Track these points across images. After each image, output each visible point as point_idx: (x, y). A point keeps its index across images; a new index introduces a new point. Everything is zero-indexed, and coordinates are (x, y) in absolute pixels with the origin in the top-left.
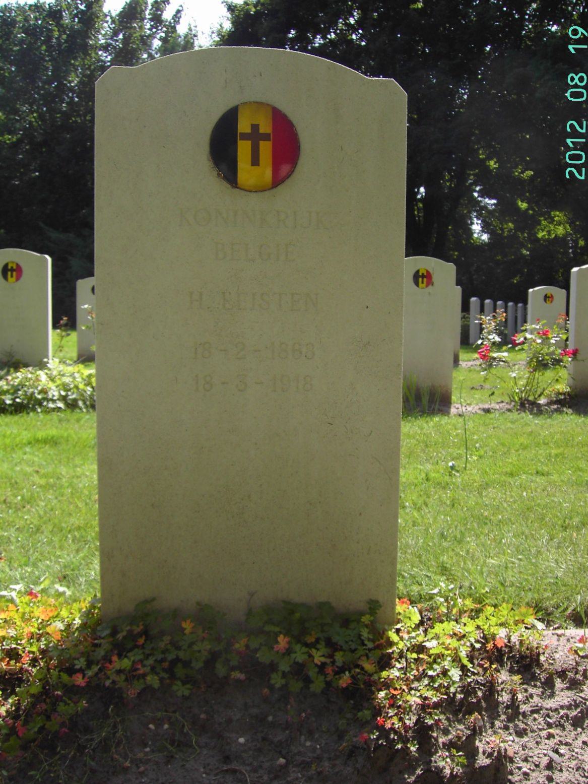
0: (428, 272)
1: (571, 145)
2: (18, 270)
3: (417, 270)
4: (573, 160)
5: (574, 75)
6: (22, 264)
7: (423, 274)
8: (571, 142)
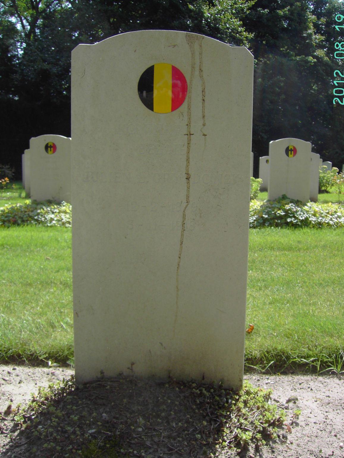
1: (336, 85)
2: (294, 151)
4: (337, 94)
5: (338, 43)
6: (56, 144)
8: (337, 83)
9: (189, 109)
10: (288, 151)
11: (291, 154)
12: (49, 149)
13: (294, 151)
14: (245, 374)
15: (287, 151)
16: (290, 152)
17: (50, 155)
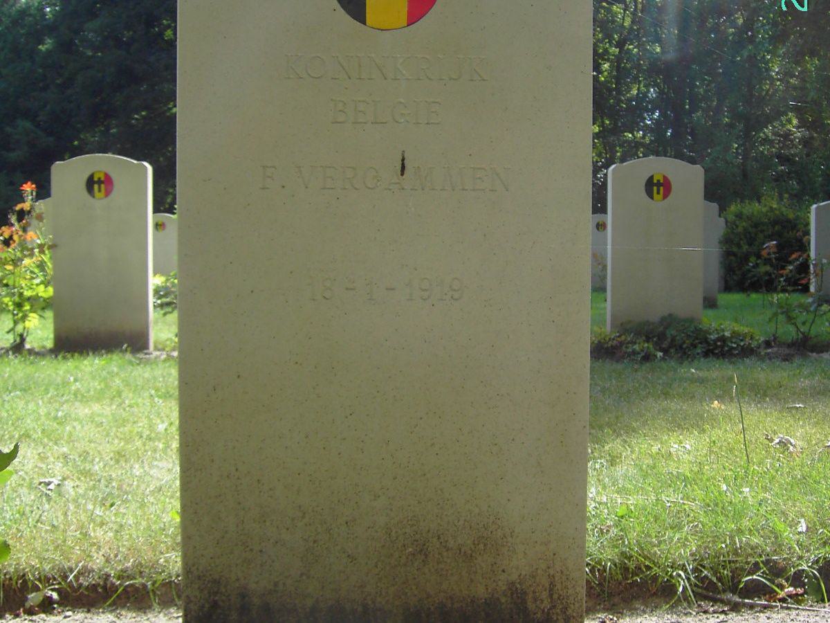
0: (665, 178)
2: (107, 181)
3: (650, 175)
7: (658, 181)
10: (651, 186)
12: (96, 187)
13: (107, 181)
14: (612, 415)
15: (650, 185)
17: (658, 202)
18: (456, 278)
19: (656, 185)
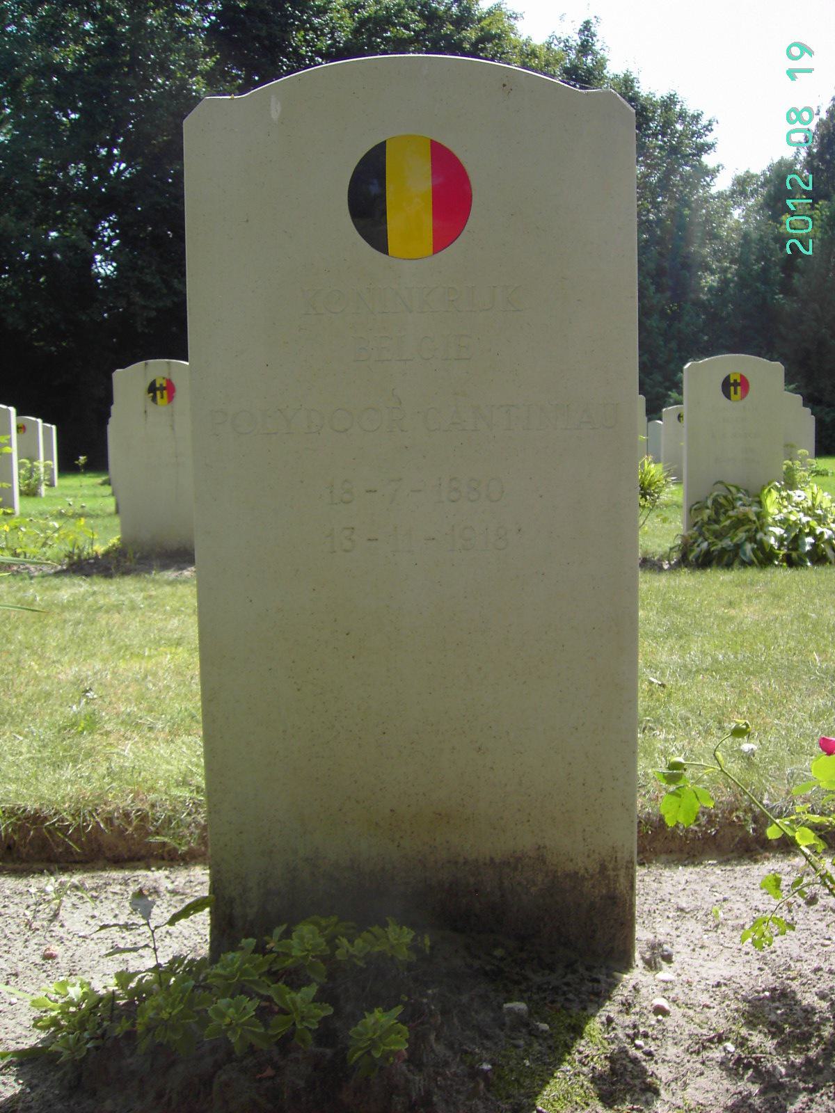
2: (744, 384)
9: (627, 810)
11: (735, 393)
13: (744, 384)
16: (732, 388)
18: (472, 501)
19: (733, 385)
